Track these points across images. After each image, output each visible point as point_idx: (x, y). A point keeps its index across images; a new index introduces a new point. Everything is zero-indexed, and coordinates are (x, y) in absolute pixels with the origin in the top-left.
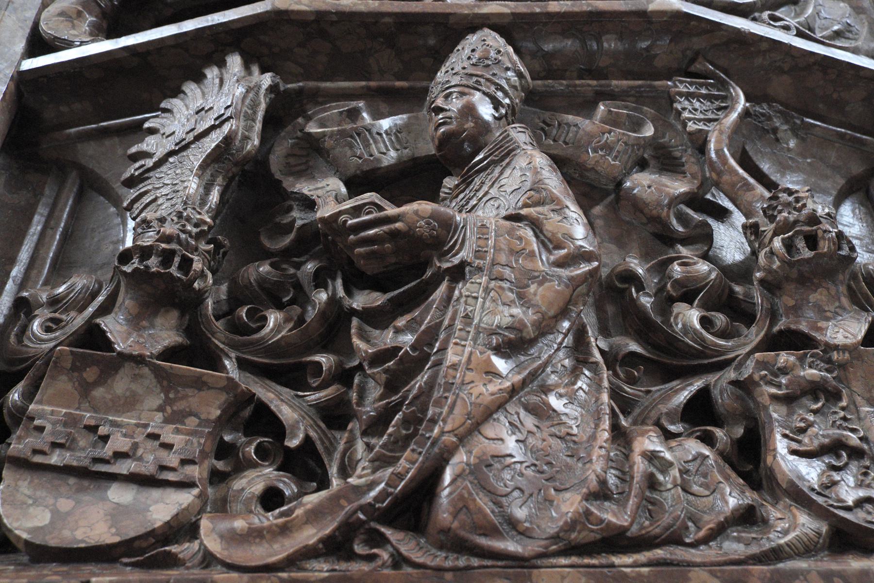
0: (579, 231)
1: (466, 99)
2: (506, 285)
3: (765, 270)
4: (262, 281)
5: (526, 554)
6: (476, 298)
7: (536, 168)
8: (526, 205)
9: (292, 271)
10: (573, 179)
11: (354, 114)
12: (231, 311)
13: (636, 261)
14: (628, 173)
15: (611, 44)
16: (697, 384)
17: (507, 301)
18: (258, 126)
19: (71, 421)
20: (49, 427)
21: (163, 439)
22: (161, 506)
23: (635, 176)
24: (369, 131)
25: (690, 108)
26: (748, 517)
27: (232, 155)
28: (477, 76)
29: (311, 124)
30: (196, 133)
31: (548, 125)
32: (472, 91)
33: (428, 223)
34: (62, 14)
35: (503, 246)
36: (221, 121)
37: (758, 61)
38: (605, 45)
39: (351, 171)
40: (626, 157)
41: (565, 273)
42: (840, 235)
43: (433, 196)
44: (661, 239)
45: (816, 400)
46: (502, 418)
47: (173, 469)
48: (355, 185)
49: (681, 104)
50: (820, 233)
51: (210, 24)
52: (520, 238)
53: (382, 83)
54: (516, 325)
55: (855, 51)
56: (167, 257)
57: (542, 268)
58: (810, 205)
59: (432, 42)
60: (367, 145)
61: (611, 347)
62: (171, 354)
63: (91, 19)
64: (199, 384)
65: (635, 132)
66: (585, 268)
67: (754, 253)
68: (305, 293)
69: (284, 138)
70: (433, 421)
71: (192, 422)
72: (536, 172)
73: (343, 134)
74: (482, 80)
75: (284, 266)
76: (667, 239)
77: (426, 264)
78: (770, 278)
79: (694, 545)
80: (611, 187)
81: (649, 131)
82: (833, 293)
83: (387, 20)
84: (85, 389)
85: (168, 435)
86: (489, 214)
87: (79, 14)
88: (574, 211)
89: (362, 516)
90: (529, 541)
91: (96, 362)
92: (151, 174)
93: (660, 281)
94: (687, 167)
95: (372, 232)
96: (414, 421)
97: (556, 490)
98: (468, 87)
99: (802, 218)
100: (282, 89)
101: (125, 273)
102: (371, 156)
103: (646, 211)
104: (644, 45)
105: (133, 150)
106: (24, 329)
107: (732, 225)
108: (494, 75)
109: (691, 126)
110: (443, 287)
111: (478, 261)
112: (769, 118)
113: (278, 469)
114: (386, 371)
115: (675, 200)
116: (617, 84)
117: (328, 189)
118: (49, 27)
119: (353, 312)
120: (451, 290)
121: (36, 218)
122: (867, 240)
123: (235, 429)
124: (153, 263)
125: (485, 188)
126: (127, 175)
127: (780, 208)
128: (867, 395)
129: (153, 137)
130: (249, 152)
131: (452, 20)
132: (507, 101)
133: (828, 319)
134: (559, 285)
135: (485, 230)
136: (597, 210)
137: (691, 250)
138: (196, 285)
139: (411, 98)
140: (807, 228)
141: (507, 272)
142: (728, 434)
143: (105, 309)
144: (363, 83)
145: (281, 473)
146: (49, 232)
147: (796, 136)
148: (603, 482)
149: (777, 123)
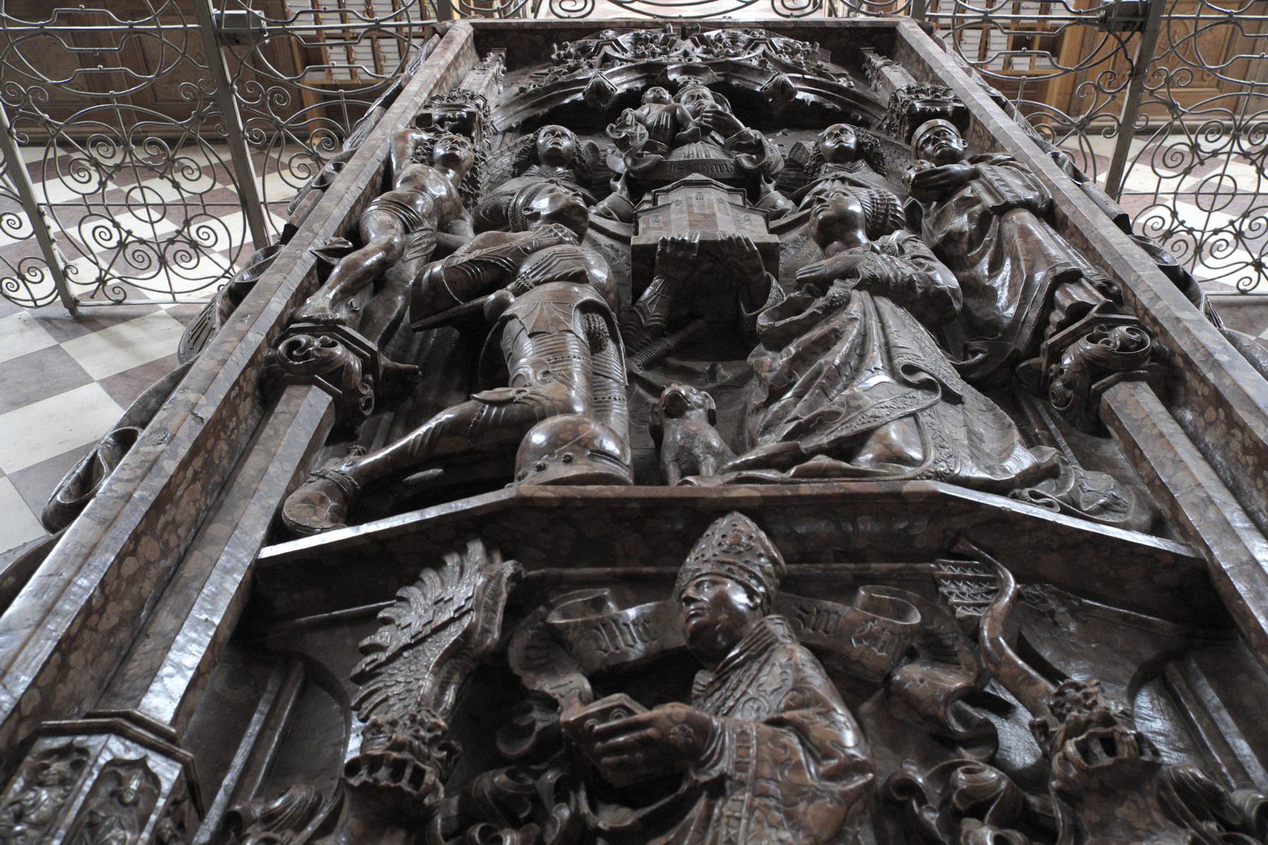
0: (849, 738)
1: (718, 588)
2: (772, 803)
3: (1061, 779)
4: (497, 792)
6: (739, 819)
7: (797, 665)
8: (788, 708)
9: (530, 781)
10: (837, 671)
11: (598, 604)
13: (914, 768)
14: (897, 665)
15: (867, 525)
17: (774, 822)
18: (499, 617)
23: (905, 668)
24: (615, 622)
27: (471, 649)
28: (729, 563)
29: (553, 613)
30: (433, 625)
31: (806, 612)
33: (683, 729)
34: (306, 500)
35: (767, 757)
36: (461, 613)
37: (1024, 540)
38: (861, 527)
39: (597, 666)
40: (893, 648)
41: (836, 787)
42: (1140, 737)
43: (684, 695)
44: (940, 743)
48: (604, 681)
49: (947, 588)
50: (1117, 736)
51: (454, 510)
52: (785, 747)
53: (630, 569)
55: (1126, 526)
56: (398, 768)
57: (811, 782)
58: (1102, 703)
59: (679, 526)
60: (613, 637)
63: (332, 504)
65: (900, 618)
66: (859, 781)
67: (1047, 757)
68: (543, 806)
72: (797, 669)
73: (587, 625)
75: (522, 775)
76: (947, 741)
77: (681, 776)
78: (1068, 788)
80: (880, 680)
81: (916, 618)
82: (1142, 806)
83: (634, 505)
86: (749, 716)
87: (322, 500)
88: (841, 714)
92: (383, 670)
93: (944, 791)
94: (960, 656)
95: (621, 739)
98: (720, 575)
99: (1094, 718)
100: (524, 576)
101: (351, 787)
102: (618, 648)
104: (902, 526)
105: (366, 642)
107: (1017, 722)
108: (747, 562)
110: (701, 804)
111: (738, 774)
112: (1044, 600)
115: (952, 696)
116: (877, 567)
117: (571, 686)
118: (291, 515)
119: (598, 832)
120: (710, 808)
121: (256, 716)
122: (1173, 737)
124: (383, 774)
125: (743, 687)
126: (357, 670)
127: (1068, 705)
129: (386, 628)
130: (488, 647)
132: (762, 589)
134: (677, 407)
135: (745, 738)
136: (866, 707)
137: (976, 754)
138: (426, 801)
139: (658, 585)
140: (1101, 730)
141: (772, 787)
144: (609, 570)
146: (269, 732)
147: (1077, 619)
149: (1053, 604)
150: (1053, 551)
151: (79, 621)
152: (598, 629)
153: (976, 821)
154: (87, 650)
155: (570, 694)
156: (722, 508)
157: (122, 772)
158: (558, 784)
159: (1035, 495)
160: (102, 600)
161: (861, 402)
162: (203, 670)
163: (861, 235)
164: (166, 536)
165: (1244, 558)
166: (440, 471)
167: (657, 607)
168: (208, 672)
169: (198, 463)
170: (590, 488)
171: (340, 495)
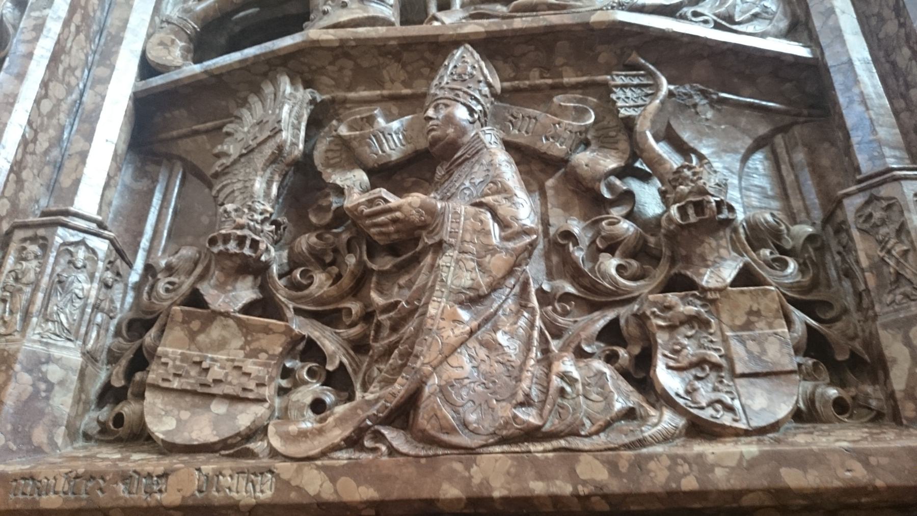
4: (311, 248)
5: (473, 446)
6: (449, 267)
11: (371, 120)
12: (290, 272)
16: (610, 315)
17: (469, 268)
18: (302, 134)
19: (184, 358)
20: (171, 363)
21: (244, 370)
22: (244, 415)
25: (623, 96)
26: (630, 414)
31: (515, 118)
32: (454, 102)
33: (418, 212)
35: (469, 227)
40: (571, 142)
41: (510, 245)
45: (693, 328)
46: (464, 351)
47: (251, 391)
52: (481, 221)
54: (475, 286)
60: (381, 145)
61: (552, 289)
62: (248, 309)
63: (182, 44)
64: (267, 330)
69: (324, 137)
70: (417, 357)
71: (263, 356)
74: (461, 93)
77: (417, 239)
79: (589, 436)
83: (392, 43)
84: (192, 335)
85: (250, 366)
89: (369, 423)
90: (476, 436)
91: (197, 317)
92: (229, 170)
96: (408, 355)
97: (497, 400)
100: (319, 100)
102: (383, 151)
103: (584, 183)
106: (152, 287)
108: (469, 88)
109: (623, 113)
110: (428, 259)
112: (691, 96)
113: (323, 385)
114: (390, 319)
120: (434, 260)
123: (294, 358)
124: (232, 247)
125: (461, 180)
128: (730, 323)
132: (479, 108)
133: (707, 266)
135: (457, 216)
139: (414, 102)
141: (471, 247)
143: (202, 277)
144: (378, 92)
145: (325, 387)
146: (164, 210)
148: (527, 395)
149: (697, 99)
150: (704, 58)
151: (20, 150)
152: (371, 139)
154: (32, 168)
155: (353, 181)
157: (71, 249)
158: (349, 242)
159: (696, 14)
160: (33, 133)
162: (111, 175)
164: (67, 79)
165: (845, 59)
166: (257, 9)
167: (412, 118)
168: (116, 175)
169: (77, 18)
170: (361, 30)
171: (185, 36)
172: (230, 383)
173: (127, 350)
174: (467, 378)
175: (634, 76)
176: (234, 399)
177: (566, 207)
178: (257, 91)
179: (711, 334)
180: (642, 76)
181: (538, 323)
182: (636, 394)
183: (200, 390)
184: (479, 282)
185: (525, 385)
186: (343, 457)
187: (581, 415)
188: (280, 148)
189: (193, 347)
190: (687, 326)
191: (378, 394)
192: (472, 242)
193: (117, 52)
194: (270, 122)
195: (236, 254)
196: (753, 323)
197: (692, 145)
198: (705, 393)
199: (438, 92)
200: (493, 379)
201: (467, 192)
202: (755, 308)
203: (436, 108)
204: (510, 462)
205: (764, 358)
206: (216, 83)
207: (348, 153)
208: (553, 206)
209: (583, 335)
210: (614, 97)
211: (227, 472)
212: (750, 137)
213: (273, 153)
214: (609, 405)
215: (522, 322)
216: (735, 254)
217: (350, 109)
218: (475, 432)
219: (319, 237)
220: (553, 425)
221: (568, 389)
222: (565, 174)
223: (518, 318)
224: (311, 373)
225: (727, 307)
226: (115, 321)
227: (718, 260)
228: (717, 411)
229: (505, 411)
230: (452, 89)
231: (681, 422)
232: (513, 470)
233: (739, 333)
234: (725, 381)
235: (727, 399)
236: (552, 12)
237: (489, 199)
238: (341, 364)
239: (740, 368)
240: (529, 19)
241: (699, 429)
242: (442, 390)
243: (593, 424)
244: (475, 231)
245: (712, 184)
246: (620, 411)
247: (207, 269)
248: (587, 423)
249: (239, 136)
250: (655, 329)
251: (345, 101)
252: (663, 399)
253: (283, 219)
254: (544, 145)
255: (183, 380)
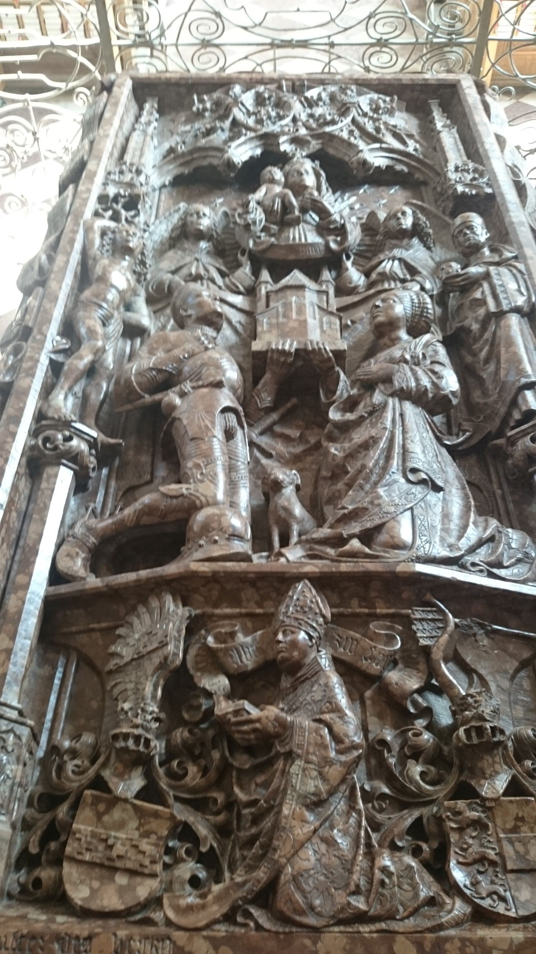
2: (312, 766)
6: (298, 775)
11: (232, 635)
16: (416, 814)
19: (94, 835)
20: (83, 839)
21: (140, 848)
25: (421, 628)
26: (431, 902)
31: (341, 638)
33: (273, 724)
41: (343, 758)
45: (476, 830)
46: (309, 846)
52: (321, 736)
54: (318, 792)
60: (240, 657)
61: (372, 788)
63: (83, 555)
69: (195, 643)
70: (275, 850)
71: (153, 838)
77: (270, 746)
79: (402, 920)
84: (99, 816)
85: (145, 845)
89: (240, 902)
96: (267, 847)
97: (335, 889)
102: (242, 662)
110: (280, 764)
112: (471, 628)
113: (197, 862)
124: (131, 743)
131: (287, 575)
133: (486, 779)
142: (429, 847)
143: (104, 765)
148: (358, 886)
149: (476, 629)
153: (414, 761)
156: (299, 578)
161: (380, 501)
163: (403, 334)
167: (263, 634)
170: (229, 564)
171: (87, 549)
172: (129, 859)
173: (38, 820)
174: (313, 869)
175: (429, 611)
176: (132, 873)
177: (380, 716)
178: (145, 602)
179: (489, 835)
180: (435, 611)
181: (364, 823)
182: (435, 884)
183: (106, 863)
184: (320, 789)
185: (355, 877)
186: (222, 930)
187: (396, 903)
188: (166, 658)
189: (100, 825)
190: (472, 828)
191: (244, 878)
192: (314, 753)
193: (34, 562)
194: (159, 635)
195: (133, 751)
196: (519, 827)
197: (473, 667)
198: (485, 886)
199: (285, 619)
200: (332, 870)
201: (310, 708)
202: (520, 815)
203: (284, 632)
204: (345, 940)
205: (527, 857)
206: (113, 594)
207: (214, 662)
208: (371, 715)
209: (396, 831)
210: (414, 627)
211: (137, 938)
212: (517, 660)
213: (160, 663)
214: (416, 895)
215: (352, 821)
216: (506, 767)
217: (215, 621)
218: (319, 914)
219: (190, 732)
220: (376, 910)
221: (387, 881)
222: (379, 688)
223: (349, 819)
224: (188, 852)
225: (500, 814)
226: (28, 793)
227: (493, 773)
228: (494, 901)
229: (341, 898)
230: (296, 619)
231: (468, 910)
232: (348, 947)
233: (509, 835)
234: (500, 876)
235: (501, 890)
236: (368, 560)
237: (327, 717)
238: (212, 847)
239: (510, 866)
240: (352, 564)
241: (481, 916)
242: (295, 878)
243: (405, 910)
244: (316, 744)
245: (488, 711)
246: (424, 900)
247: (108, 759)
248: (401, 909)
249: (131, 641)
250: (449, 830)
251: (212, 615)
252: (453, 889)
253: (163, 716)
254: (364, 664)
255: (93, 854)
